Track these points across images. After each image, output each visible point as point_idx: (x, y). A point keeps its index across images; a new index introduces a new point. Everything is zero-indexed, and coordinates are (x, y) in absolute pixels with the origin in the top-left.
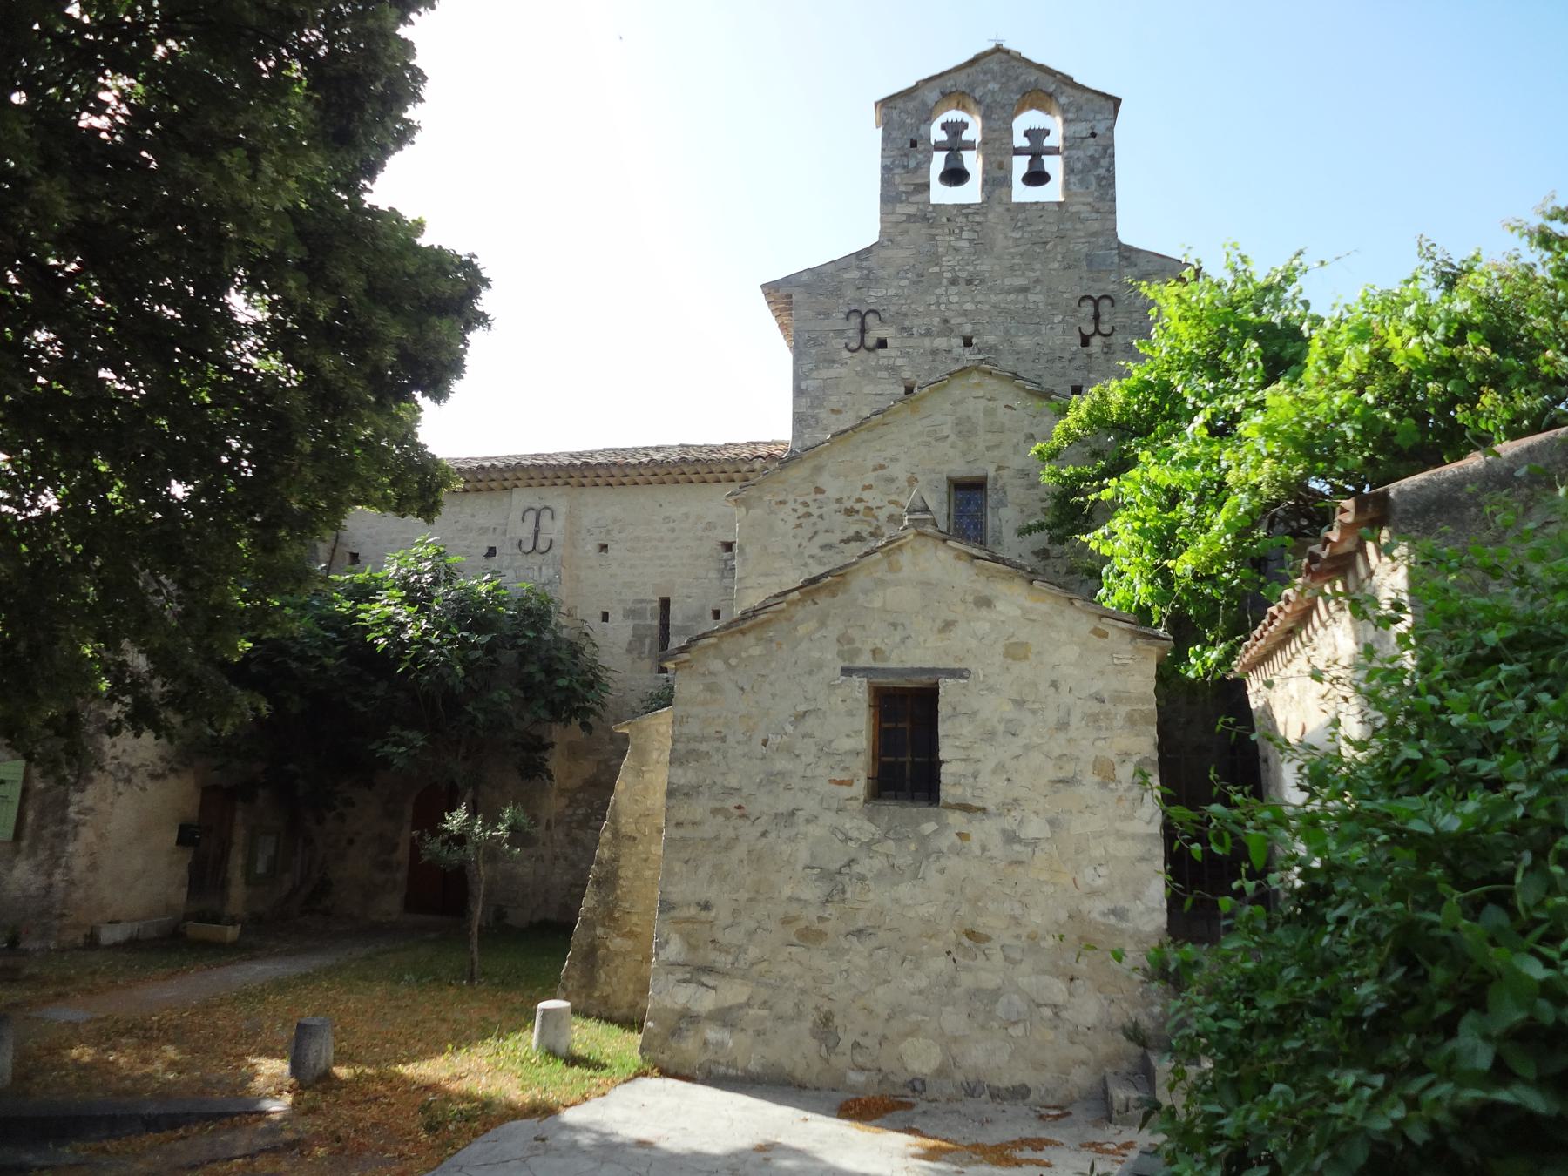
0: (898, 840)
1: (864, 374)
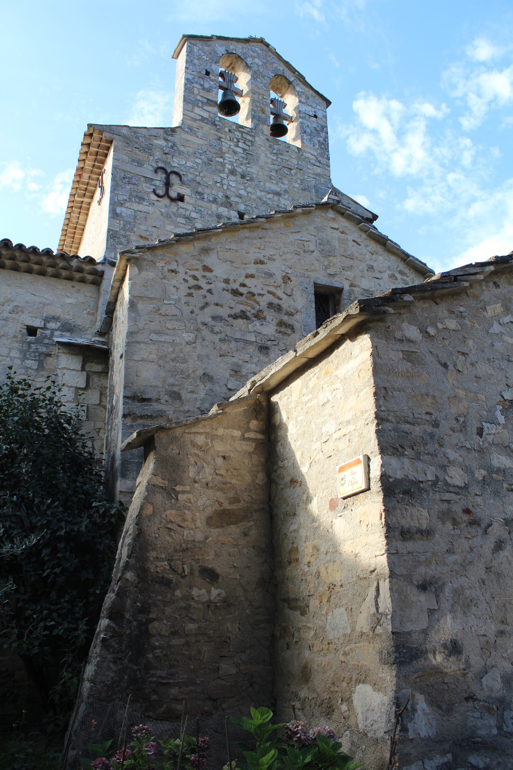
1: (168, 216)
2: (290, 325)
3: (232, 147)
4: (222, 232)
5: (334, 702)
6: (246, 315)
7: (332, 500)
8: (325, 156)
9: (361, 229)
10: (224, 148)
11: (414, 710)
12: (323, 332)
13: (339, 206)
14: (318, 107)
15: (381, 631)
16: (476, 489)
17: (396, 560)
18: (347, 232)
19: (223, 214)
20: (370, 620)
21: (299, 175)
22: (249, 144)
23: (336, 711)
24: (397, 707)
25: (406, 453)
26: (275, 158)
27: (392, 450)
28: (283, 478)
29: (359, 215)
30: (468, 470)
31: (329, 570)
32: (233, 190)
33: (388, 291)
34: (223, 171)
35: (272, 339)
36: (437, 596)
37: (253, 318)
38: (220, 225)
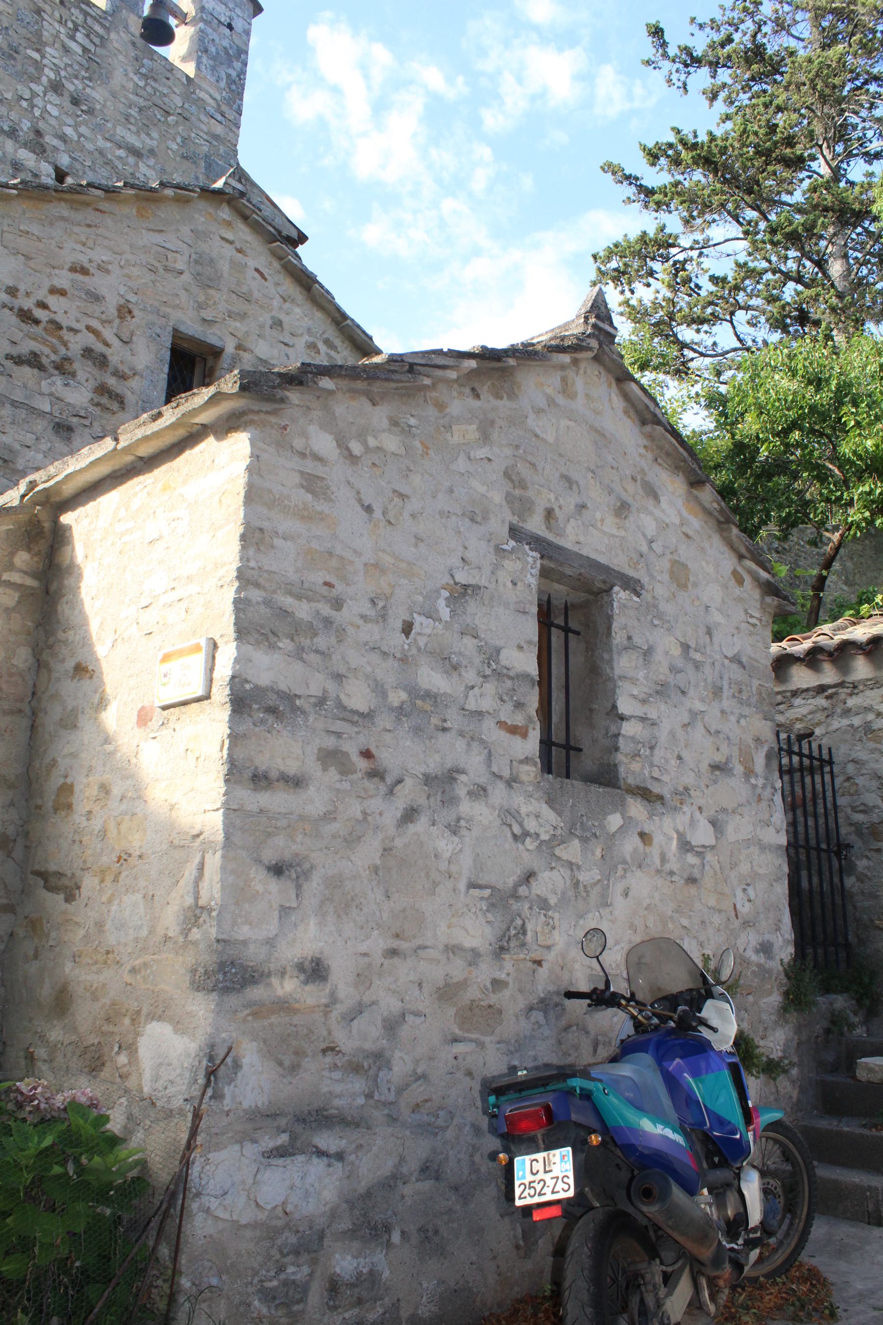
0: (584, 840)
2: (117, 395)
3: (63, 37)
4: (18, 196)
5: (106, 1050)
6: (40, 362)
7: (143, 708)
8: (235, 107)
9: (273, 253)
10: (45, 33)
11: (237, 1066)
12: (170, 415)
13: (244, 203)
14: (238, 11)
15: (198, 936)
16: (384, 721)
17: (238, 821)
18: (248, 251)
19: (25, 163)
20: (182, 918)
21: (180, 128)
22: (97, 41)
23: (108, 1064)
24: (209, 1061)
25: (281, 645)
26: (142, 84)
27: (256, 636)
28: (63, 661)
29: (274, 228)
30: (380, 690)
31: (124, 827)
32: (53, 122)
33: (294, 365)
34: (37, 80)
35: (82, 413)
36: (299, 887)
37: (52, 371)
38: (15, 181)
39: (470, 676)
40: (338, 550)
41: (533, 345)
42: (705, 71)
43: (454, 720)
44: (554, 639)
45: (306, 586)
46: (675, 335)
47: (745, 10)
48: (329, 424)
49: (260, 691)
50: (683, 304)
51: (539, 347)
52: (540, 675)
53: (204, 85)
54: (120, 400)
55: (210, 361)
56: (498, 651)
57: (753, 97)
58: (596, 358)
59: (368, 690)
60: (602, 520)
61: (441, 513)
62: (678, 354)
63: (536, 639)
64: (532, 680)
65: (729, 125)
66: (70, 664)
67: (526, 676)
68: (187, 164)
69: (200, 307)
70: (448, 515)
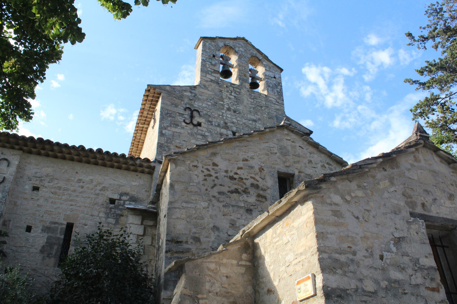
1: (192, 135)
2: (264, 196)
8: (281, 99)
9: (303, 140)
12: (284, 201)
14: (276, 73)
16: (381, 294)
22: (238, 93)
25: (337, 272)
26: (252, 101)
27: (329, 270)
28: (263, 289)
30: (377, 282)
33: (321, 176)
34: (223, 109)
35: (254, 205)
37: (242, 193)
39: (410, 271)
40: (350, 234)
41: (400, 148)
42: (431, 40)
43: (408, 290)
44: (438, 251)
45: (342, 249)
46: (450, 128)
47: (438, 18)
48: (337, 192)
49: (334, 290)
50: (449, 117)
51: (402, 148)
52: (437, 266)
53: (271, 96)
54: (265, 198)
55: (291, 179)
56: (418, 260)
57: (451, 43)
58: (424, 146)
59: (373, 283)
60: (444, 203)
61: (383, 214)
62: (453, 134)
63: (432, 252)
64: (435, 268)
65: (446, 54)
66: (266, 290)
67: (432, 268)
68: (271, 120)
69: (284, 162)
70: (386, 214)
